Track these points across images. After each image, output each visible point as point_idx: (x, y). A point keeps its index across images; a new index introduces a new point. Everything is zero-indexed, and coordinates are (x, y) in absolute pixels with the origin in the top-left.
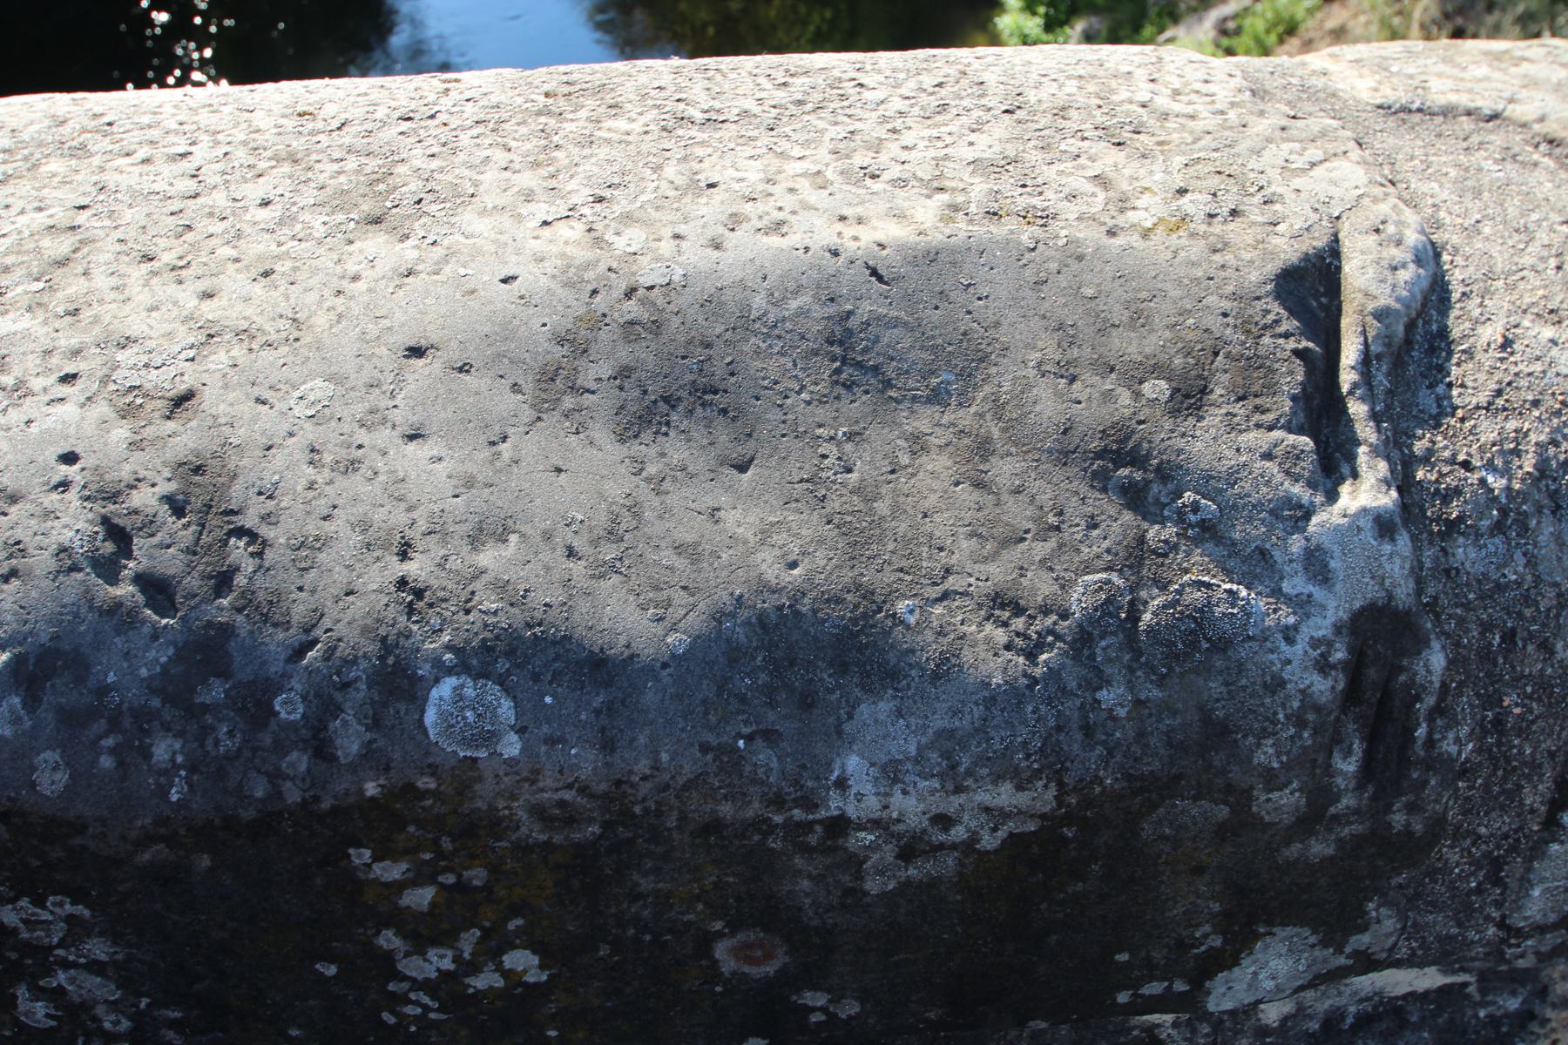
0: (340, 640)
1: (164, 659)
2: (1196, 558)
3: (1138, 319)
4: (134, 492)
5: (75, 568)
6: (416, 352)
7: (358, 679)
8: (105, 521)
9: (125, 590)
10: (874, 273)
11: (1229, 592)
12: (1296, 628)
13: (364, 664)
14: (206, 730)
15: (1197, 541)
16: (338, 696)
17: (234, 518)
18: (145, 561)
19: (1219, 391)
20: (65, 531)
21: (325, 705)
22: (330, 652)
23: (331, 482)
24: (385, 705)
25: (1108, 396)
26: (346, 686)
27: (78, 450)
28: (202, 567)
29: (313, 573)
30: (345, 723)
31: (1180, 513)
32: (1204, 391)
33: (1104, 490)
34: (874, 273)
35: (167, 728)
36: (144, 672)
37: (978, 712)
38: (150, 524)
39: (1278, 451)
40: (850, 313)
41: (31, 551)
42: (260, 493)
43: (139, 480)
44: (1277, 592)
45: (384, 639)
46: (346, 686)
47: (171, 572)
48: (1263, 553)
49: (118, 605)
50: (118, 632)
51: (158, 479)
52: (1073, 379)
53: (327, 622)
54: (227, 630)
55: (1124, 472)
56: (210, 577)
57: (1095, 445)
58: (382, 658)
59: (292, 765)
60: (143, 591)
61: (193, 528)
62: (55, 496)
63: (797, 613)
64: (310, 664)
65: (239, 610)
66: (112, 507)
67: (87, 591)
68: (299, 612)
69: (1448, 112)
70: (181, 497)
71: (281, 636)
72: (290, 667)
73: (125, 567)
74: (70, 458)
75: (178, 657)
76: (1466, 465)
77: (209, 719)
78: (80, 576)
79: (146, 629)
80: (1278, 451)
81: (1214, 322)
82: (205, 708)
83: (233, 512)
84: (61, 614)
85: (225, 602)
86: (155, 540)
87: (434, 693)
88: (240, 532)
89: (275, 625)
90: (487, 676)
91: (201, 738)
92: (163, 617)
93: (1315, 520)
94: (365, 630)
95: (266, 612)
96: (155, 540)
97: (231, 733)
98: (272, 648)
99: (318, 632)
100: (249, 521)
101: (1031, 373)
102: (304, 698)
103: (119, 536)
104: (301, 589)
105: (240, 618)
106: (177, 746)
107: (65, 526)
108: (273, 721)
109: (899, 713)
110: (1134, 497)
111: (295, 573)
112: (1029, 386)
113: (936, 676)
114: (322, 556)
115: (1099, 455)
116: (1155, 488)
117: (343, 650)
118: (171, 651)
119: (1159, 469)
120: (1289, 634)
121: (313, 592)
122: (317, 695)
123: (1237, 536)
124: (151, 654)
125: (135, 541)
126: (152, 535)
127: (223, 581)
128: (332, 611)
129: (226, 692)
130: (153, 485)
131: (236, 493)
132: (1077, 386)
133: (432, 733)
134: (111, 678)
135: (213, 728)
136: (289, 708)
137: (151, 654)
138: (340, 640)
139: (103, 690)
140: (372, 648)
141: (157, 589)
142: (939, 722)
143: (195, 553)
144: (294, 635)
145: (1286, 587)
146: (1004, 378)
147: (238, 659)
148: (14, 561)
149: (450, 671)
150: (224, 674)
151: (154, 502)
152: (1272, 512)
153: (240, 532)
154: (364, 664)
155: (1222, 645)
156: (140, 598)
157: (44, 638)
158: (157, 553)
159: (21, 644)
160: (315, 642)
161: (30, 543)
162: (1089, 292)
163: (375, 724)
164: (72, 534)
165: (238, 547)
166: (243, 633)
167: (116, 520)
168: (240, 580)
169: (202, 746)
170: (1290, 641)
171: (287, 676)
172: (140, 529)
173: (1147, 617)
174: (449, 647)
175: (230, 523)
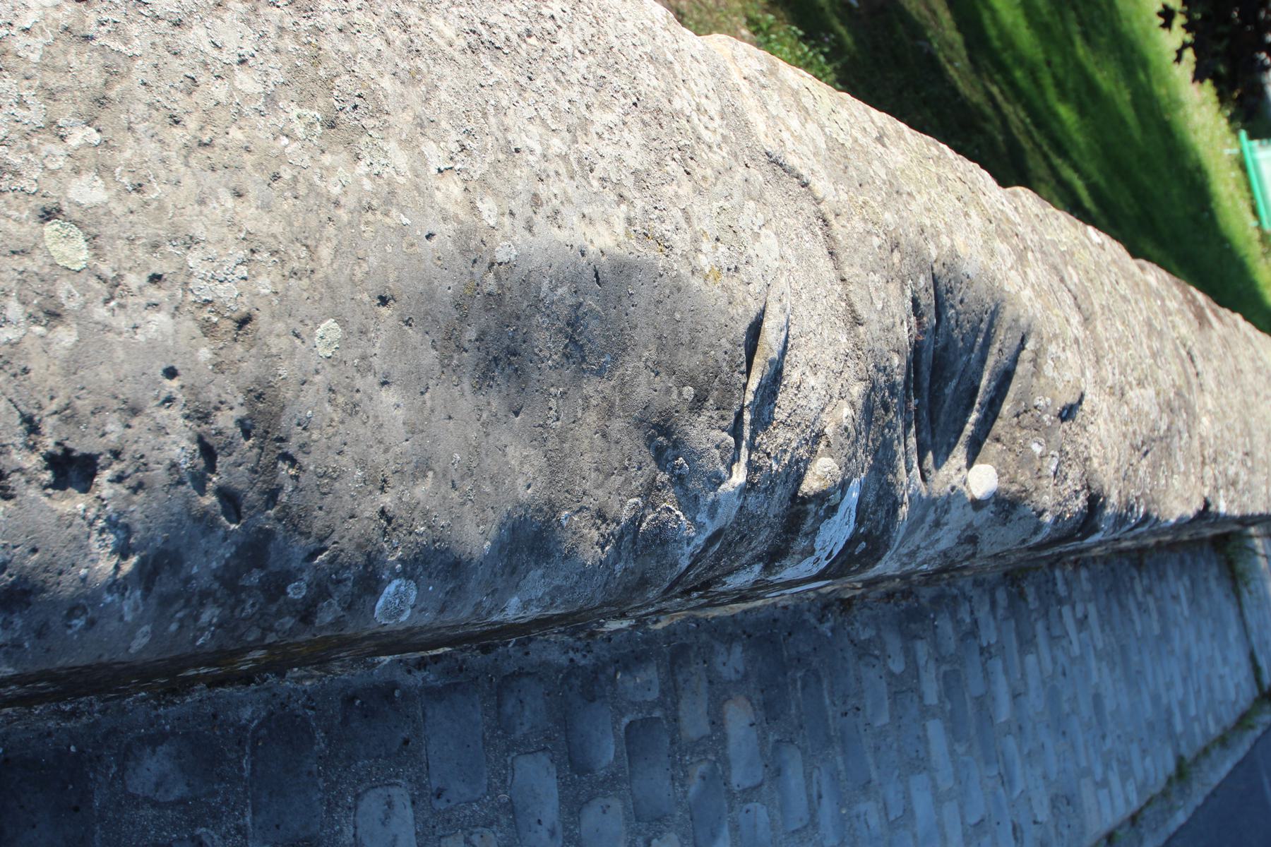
0: (342, 551)
1: (228, 555)
2: (671, 494)
3: (692, 345)
4: (219, 414)
5: (181, 482)
6: (384, 301)
7: (348, 579)
8: (200, 440)
9: (209, 500)
10: (596, 275)
11: (678, 516)
12: (693, 538)
13: (354, 569)
14: (240, 602)
15: (674, 485)
16: (331, 587)
17: (283, 445)
18: (225, 476)
19: (711, 401)
20: (174, 447)
21: (321, 591)
22: (332, 560)
23: (342, 422)
24: (360, 597)
25: (668, 391)
26: (339, 582)
27: (177, 366)
28: (259, 485)
29: (330, 498)
30: (330, 605)
31: (674, 468)
32: (705, 400)
33: (649, 447)
34: (596, 275)
35: (215, 601)
36: (214, 565)
37: (576, 578)
38: (229, 446)
39: (723, 445)
40: (581, 304)
41: (152, 465)
42: (299, 425)
43: (222, 403)
44: (693, 519)
45: (369, 554)
46: (339, 582)
47: (240, 487)
48: (696, 497)
49: (206, 512)
50: (204, 534)
51: (235, 404)
52: (657, 374)
53: (335, 537)
54: (270, 534)
55: (661, 439)
56: (265, 493)
57: (655, 420)
58: (365, 567)
59: (283, 624)
60: (221, 501)
61: (256, 450)
62: (164, 412)
63: (526, 519)
64: (318, 564)
65: (280, 520)
66: (205, 427)
67: (187, 502)
68: (318, 526)
69: (789, 171)
70: (248, 422)
71: (303, 542)
72: (305, 564)
73: (210, 480)
74: (171, 373)
75: (236, 555)
76: (768, 455)
77: (243, 596)
78: (183, 488)
79: (221, 533)
80: (723, 445)
81: (720, 355)
82: (244, 588)
83: (281, 440)
84: (171, 521)
85: (271, 512)
86: (232, 459)
87: (387, 590)
88: (286, 457)
89: (301, 534)
90: (411, 578)
91: (233, 609)
92: (232, 522)
93: (723, 486)
94: (359, 546)
95: (294, 522)
96: (232, 459)
97: (253, 605)
98: (296, 550)
99: (328, 543)
100: (291, 447)
101: (642, 364)
102: (308, 586)
103: (208, 452)
104: (320, 508)
105: (279, 527)
106: (217, 612)
107: (174, 443)
108: (282, 598)
109: (543, 576)
110: (660, 456)
111: (317, 495)
112: (638, 374)
113: (566, 557)
114: (337, 485)
115: (655, 426)
116: (669, 451)
117: (343, 558)
118: (233, 549)
119: (675, 441)
120: (690, 540)
121: (328, 513)
122: (318, 585)
123: (690, 486)
124: (221, 552)
125: (219, 459)
126: (230, 455)
127: (272, 496)
128: (339, 529)
129: (260, 579)
130: (231, 409)
131: (284, 422)
132: (658, 379)
133: (377, 612)
134: (195, 570)
135: (244, 602)
136: (296, 592)
137: (221, 552)
138: (342, 551)
139: (188, 579)
140: (361, 559)
141: (229, 498)
142: (557, 582)
143: (256, 472)
144: (312, 543)
145: (698, 519)
146: (630, 365)
147: (273, 556)
148: (140, 475)
149: (397, 576)
150: (262, 567)
151: (231, 424)
152: (709, 479)
153: (286, 457)
154: (354, 569)
155: (664, 543)
156: (219, 507)
157: (159, 542)
158: (233, 470)
159: (145, 548)
160: (326, 549)
161: (152, 456)
162: (678, 316)
163: (349, 607)
164: (178, 451)
165: (284, 469)
166: (280, 538)
167: (207, 440)
168: (283, 498)
169: (232, 612)
170: (688, 544)
171: (301, 570)
172: (223, 449)
173: (644, 525)
174: (400, 560)
175: (279, 448)
